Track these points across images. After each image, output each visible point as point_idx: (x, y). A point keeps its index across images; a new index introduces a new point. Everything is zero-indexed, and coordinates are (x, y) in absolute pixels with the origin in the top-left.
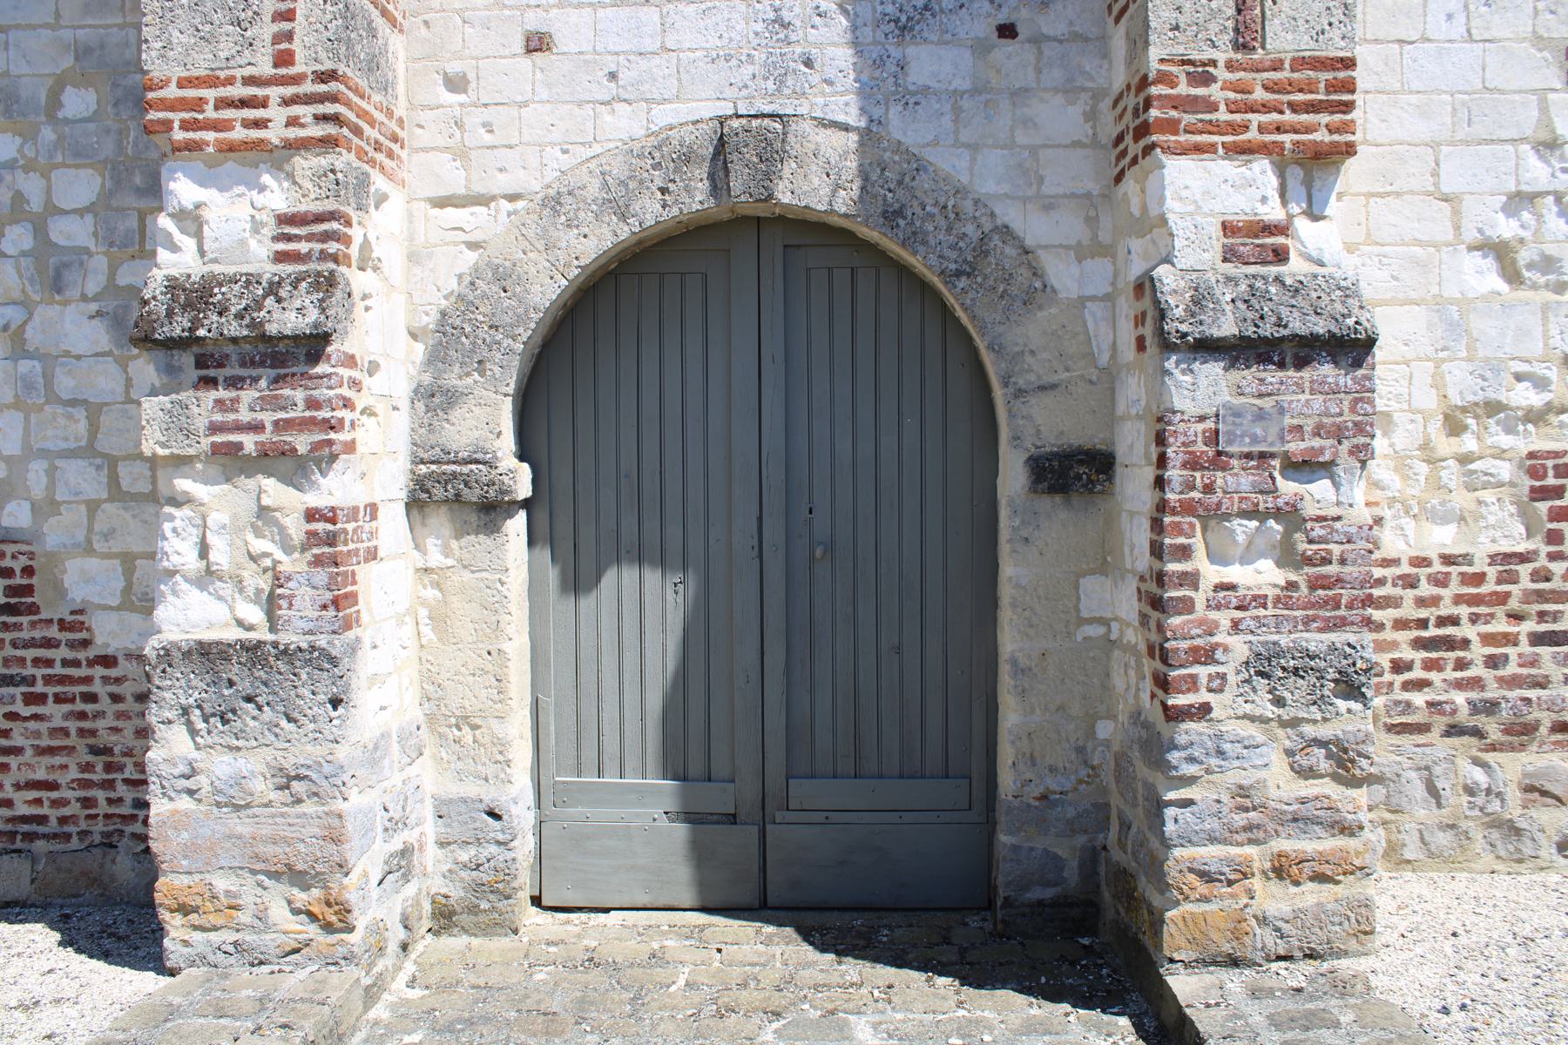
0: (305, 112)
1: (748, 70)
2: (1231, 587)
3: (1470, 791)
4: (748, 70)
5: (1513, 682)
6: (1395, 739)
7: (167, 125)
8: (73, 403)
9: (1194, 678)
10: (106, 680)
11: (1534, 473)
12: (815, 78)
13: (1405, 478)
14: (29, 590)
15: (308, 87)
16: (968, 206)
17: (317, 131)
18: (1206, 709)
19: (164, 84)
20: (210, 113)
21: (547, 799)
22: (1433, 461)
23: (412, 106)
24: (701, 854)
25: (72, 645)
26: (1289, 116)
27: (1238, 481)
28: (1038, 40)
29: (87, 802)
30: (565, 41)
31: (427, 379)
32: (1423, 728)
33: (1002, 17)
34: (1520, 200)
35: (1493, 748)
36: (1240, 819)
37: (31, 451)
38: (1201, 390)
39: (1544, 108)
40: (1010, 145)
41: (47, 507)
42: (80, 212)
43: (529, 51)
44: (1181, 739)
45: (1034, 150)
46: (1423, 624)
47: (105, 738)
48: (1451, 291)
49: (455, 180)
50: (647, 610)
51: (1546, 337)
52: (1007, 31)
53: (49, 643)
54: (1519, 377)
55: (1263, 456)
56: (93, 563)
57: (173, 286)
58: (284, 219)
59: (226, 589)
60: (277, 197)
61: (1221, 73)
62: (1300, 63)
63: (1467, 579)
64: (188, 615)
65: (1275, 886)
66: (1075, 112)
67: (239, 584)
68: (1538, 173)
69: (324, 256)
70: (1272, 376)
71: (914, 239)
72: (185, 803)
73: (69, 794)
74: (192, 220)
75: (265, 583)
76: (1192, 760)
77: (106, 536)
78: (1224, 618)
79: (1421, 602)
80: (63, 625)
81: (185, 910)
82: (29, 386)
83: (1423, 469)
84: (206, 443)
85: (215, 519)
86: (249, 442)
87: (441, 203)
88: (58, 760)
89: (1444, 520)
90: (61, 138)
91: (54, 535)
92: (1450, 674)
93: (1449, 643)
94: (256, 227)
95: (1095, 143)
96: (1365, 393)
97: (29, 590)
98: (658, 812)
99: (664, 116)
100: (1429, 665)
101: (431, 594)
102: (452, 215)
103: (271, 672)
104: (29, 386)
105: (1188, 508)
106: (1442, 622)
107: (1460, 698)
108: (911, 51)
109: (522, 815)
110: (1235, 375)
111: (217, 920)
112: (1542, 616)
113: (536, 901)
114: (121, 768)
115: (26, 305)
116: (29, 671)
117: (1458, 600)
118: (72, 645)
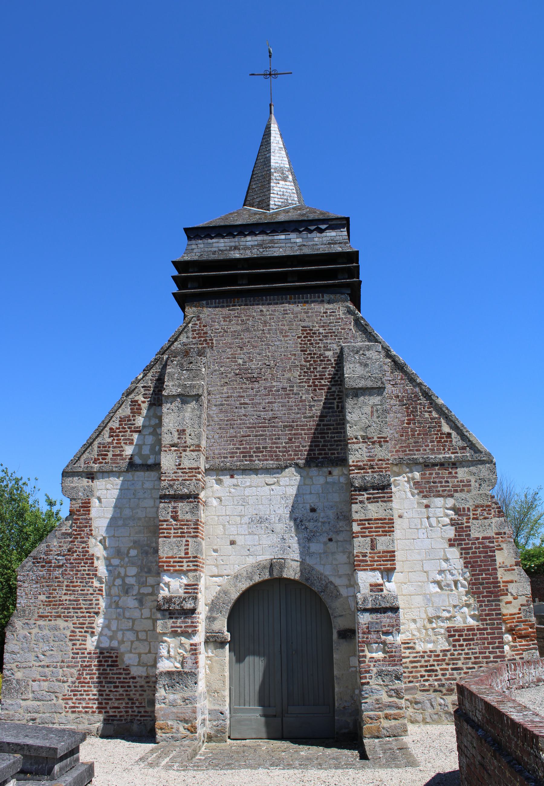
0: (191, 564)
1: (277, 549)
2: (373, 658)
3: (440, 705)
4: (277, 549)
5: (448, 679)
6: (422, 693)
7: (163, 566)
8: (129, 619)
9: (366, 677)
10: (133, 682)
11: (449, 631)
12: (291, 550)
13: (420, 633)
14: (116, 661)
15: (191, 559)
16: (323, 577)
17: (193, 568)
18: (368, 683)
19: (163, 558)
20: (172, 564)
21: (232, 711)
22: (426, 629)
23: (206, 556)
24: (268, 725)
25: (126, 674)
26: (382, 562)
27: (373, 636)
28: (337, 541)
29: (127, 712)
30: (239, 542)
31: (209, 614)
32: (428, 690)
33: (329, 537)
34: (441, 572)
35: (445, 695)
36: (377, 706)
37: (118, 630)
38: (364, 619)
39: (444, 552)
40: (332, 564)
41: (122, 642)
42: (133, 576)
43: (231, 544)
44: (364, 689)
45: (337, 565)
46: (427, 666)
47: (132, 696)
48: (427, 592)
49: (215, 571)
50: (255, 666)
51: (449, 601)
52: (331, 540)
53: (121, 674)
54: (444, 610)
55: (378, 631)
56: (131, 655)
57: (164, 598)
58: (186, 585)
59: (173, 660)
60: (185, 581)
61: (368, 555)
62: (384, 552)
63: (436, 656)
64: (165, 665)
65: (386, 721)
66: (345, 556)
67: (176, 659)
68: (444, 565)
69: (194, 593)
70: (379, 615)
71: (313, 584)
72: (163, 705)
73: (122, 710)
74: (168, 585)
75: (181, 659)
76: (366, 693)
77: (135, 649)
78: (372, 664)
79: (426, 661)
80: (124, 669)
81: (161, 729)
82: (119, 615)
83: (424, 631)
84: (170, 630)
85: (171, 645)
86: (179, 630)
87: (212, 576)
88: (120, 702)
89: (430, 642)
90: (129, 561)
91: (123, 648)
92: (434, 678)
93: (433, 671)
94: (181, 587)
95: (349, 563)
96: (398, 618)
97: (116, 661)
98: (258, 715)
99: (260, 558)
100: (429, 676)
101: (209, 662)
102: (215, 579)
103: (183, 677)
104: (119, 615)
105: (363, 642)
106: (431, 666)
107: (436, 683)
108: (311, 544)
109: (227, 713)
110: (371, 615)
111: (167, 731)
112: (453, 664)
113: (229, 737)
114: (135, 703)
115: (119, 596)
116: (115, 680)
117: (434, 661)
118: (126, 674)
